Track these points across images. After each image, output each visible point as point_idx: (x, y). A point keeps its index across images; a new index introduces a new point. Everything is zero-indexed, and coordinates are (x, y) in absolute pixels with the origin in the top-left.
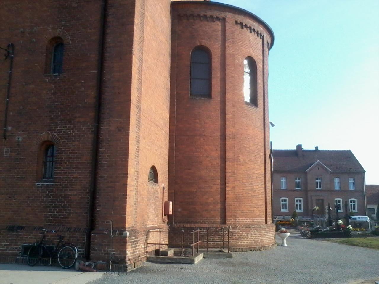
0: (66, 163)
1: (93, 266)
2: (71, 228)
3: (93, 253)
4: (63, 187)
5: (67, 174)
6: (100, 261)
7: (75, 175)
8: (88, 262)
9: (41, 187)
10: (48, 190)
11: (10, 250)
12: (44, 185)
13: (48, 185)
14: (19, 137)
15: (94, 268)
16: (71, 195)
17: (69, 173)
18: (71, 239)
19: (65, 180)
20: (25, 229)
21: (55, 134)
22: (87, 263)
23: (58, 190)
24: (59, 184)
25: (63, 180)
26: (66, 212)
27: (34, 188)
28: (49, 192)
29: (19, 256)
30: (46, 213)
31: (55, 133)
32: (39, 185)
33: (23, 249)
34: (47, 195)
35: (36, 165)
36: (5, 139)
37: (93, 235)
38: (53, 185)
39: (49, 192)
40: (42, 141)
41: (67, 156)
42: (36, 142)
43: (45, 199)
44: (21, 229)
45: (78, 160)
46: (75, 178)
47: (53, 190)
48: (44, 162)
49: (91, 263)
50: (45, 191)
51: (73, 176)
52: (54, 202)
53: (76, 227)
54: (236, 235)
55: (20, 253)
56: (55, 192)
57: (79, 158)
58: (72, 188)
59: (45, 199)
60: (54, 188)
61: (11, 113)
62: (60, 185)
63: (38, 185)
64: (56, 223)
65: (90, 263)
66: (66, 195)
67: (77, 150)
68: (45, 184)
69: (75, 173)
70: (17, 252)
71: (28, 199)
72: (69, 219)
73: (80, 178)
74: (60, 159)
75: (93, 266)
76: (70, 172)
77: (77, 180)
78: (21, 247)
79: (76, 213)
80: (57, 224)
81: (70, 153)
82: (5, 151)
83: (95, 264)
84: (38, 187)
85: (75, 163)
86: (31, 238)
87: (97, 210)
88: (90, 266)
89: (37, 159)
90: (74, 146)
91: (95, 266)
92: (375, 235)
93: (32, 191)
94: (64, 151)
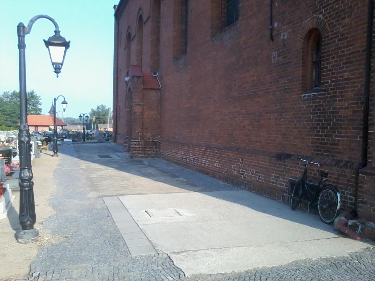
0: (334, 58)
1: (360, 228)
2: (342, 161)
3: (361, 207)
4: (331, 97)
5: (336, 75)
6: (372, 223)
7: (346, 75)
8: (352, 221)
9: (307, 99)
10: (315, 103)
11: (279, 184)
12: (310, 96)
13: (314, 95)
14: (284, 33)
15: (360, 234)
16: (341, 108)
17: (338, 73)
18: (340, 178)
19: (334, 85)
20: (291, 158)
21: (321, 16)
22: (350, 223)
23: (325, 101)
24: (326, 92)
25: (330, 86)
26: (336, 136)
27: (300, 102)
28: (316, 106)
29: (287, 193)
30: (313, 137)
31: (321, 13)
32: (305, 96)
33: (290, 185)
34: (314, 110)
35: (301, 68)
36: (272, 40)
37: (361, 175)
38: (320, 95)
39: (316, 106)
40: (306, 32)
41: (336, 45)
42: (300, 36)
43: (311, 116)
44: (288, 158)
45: (350, 50)
46: (345, 80)
47: (320, 102)
48: (314, 62)
49: (358, 223)
50: (311, 105)
51: (343, 77)
52: (321, 121)
53: (347, 160)
54: (285, 175)
55: (287, 189)
56: (322, 106)
57: (350, 46)
58: (342, 96)
59: (311, 116)
60: (320, 99)
61: (276, 4)
62: (328, 94)
63: (304, 97)
64: (324, 151)
65: (356, 223)
66: (336, 108)
67: (348, 33)
68: (311, 94)
69: (346, 72)
70: (284, 187)
71: (295, 118)
72: (340, 147)
73: (352, 79)
74: (327, 54)
75: (360, 228)
76: (339, 71)
77: (348, 83)
78: (288, 181)
79: (348, 137)
80: (325, 153)
81: (339, 40)
82: (273, 56)
83: (363, 226)
84: (305, 100)
85: (346, 55)
86: (297, 171)
87: (369, 131)
88: (354, 228)
89: (303, 59)
90: (344, 26)
91: (362, 230)
92: (31, 148)
93: (298, 106)
94: (332, 39)
